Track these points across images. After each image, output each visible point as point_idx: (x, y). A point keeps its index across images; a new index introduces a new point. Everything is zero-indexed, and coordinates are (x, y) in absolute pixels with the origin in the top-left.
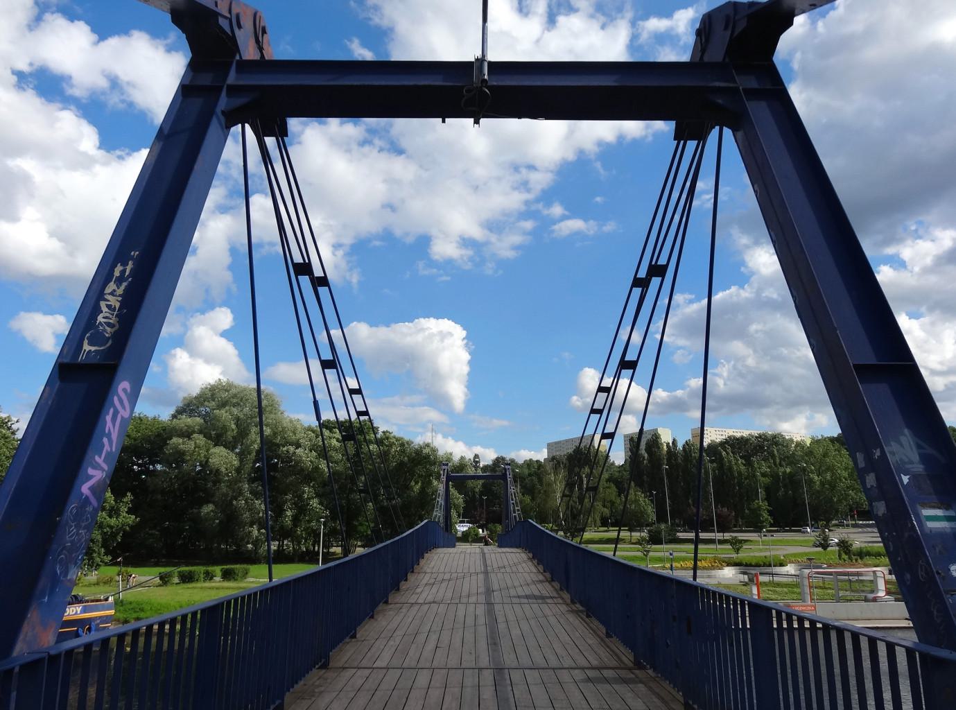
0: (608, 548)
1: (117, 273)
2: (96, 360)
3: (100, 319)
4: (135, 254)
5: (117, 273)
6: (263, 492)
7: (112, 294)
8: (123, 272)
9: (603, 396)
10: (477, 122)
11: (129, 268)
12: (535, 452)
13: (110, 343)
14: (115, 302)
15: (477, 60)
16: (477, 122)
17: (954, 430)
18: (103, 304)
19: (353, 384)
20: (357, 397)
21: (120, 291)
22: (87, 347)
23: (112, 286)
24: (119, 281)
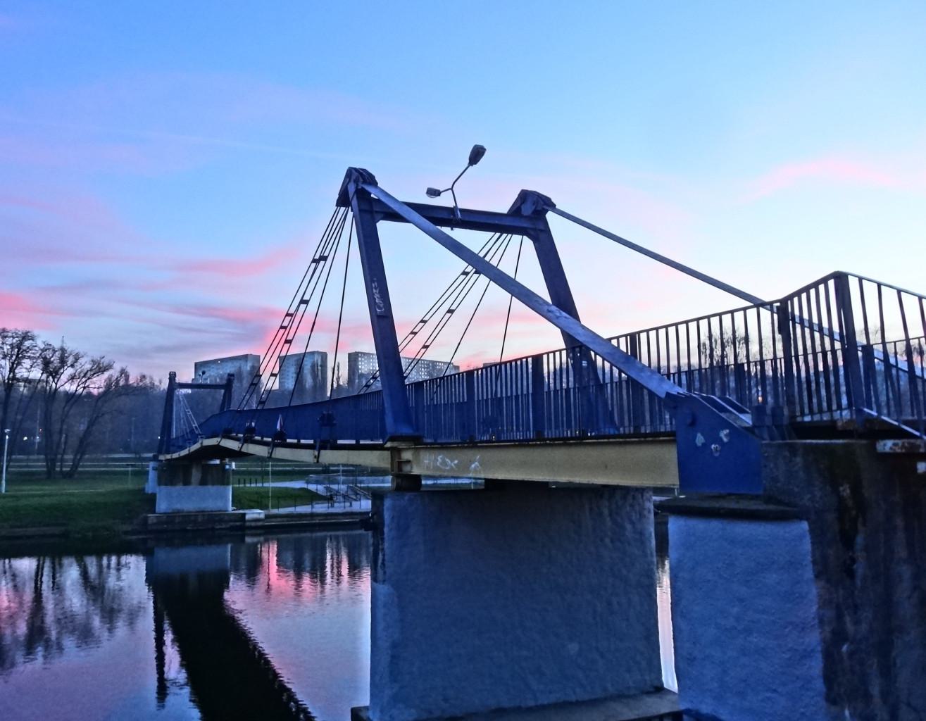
10: (452, 229)
21: (378, 292)
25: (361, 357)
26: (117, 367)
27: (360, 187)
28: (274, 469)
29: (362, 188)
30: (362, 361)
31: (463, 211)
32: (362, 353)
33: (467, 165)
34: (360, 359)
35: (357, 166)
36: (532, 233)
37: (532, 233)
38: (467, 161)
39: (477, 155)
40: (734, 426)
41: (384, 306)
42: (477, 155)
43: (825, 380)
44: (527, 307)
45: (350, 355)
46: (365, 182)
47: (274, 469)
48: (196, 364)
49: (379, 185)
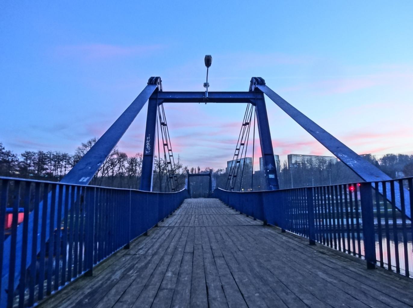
0: (80, 250)
1: (147, 139)
2: (148, 154)
3: (147, 147)
4: (149, 135)
5: (147, 139)
6: (241, 187)
7: (148, 142)
8: (148, 138)
9: (238, 151)
10: (206, 104)
11: (149, 137)
12: (409, 276)
13: (150, 151)
14: (148, 144)
15: (206, 91)
16: (206, 104)
17: (412, 156)
18: (147, 144)
19: (170, 149)
20: (170, 152)
21: (149, 142)
22: (147, 152)
23: (147, 141)
24: (148, 140)
25: (293, 156)
26: (184, 167)
27: (256, 87)
28: (313, 189)
29: (257, 87)
30: (293, 158)
31: (209, 93)
32: (293, 155)
33: (207, 68)
34: (293, 157)
35: (256, 76)
36: (252, 100)
37: (252, 100)
38: (206, 68)
39: (208, 61)
40: (63, 262)
41: (150, 150)
42: (208, 61)
43: (346, 192)
44: (312, 136)
45: (288, 156)
46: (258, 84)
47: (313, 189)
48: (228, 162)
49: (266, 84)
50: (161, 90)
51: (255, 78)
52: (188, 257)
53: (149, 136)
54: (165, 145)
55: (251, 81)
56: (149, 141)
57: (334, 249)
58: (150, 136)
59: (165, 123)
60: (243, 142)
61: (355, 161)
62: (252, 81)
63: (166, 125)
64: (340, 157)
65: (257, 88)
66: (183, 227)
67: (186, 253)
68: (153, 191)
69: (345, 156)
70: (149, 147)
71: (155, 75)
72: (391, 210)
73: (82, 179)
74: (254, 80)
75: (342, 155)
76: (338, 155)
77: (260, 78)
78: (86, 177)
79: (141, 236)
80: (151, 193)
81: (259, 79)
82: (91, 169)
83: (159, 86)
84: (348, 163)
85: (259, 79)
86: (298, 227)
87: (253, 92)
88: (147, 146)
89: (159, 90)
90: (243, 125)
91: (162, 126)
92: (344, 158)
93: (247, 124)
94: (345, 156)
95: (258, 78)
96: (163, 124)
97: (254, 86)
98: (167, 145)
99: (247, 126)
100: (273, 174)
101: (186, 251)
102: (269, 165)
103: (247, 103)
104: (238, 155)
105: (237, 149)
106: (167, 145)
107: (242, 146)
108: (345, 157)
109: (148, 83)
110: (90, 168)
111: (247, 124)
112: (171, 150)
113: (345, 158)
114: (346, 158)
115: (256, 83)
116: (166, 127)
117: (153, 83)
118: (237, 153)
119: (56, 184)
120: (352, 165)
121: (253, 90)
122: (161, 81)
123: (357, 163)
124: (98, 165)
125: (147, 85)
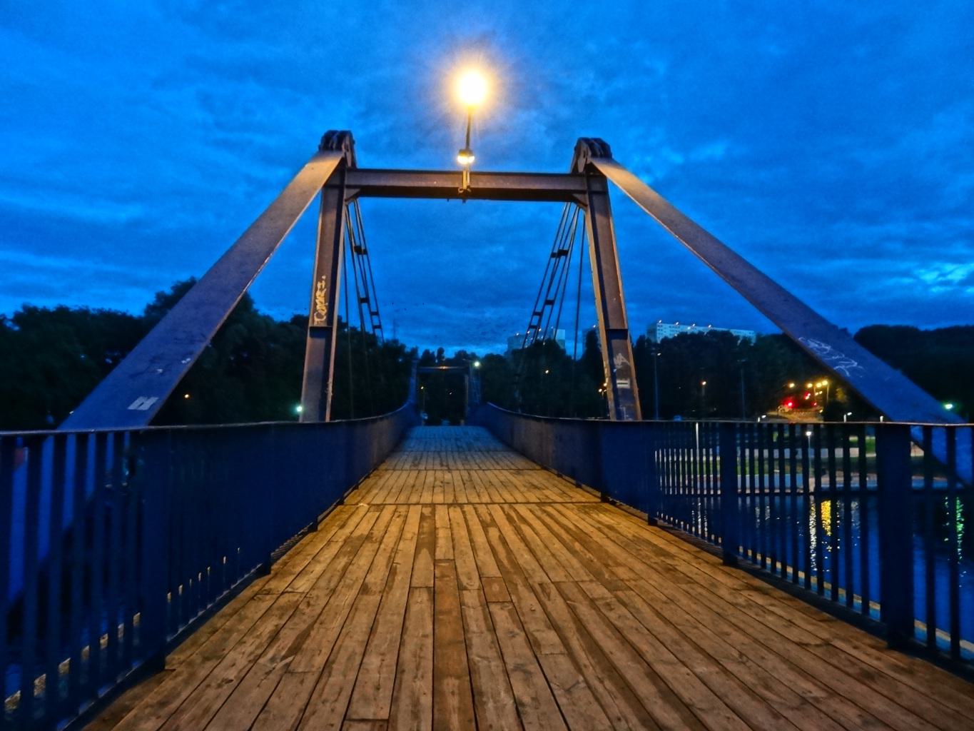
3: (318, 307)
5: (319, 287)
8: (321, 286)
19: (374, 309)
20: (375, 318)
27: (588, 162)
46: (594, 155)
49: (613, 157)
50: (354, 164)
51: (587, 140)
52: (422, 598)
53: (322, 280)
54: (362, 301)
55: (576, 149)
56: (324, 292)
57: (616, 420)
58: (326, 281)
59: (363, 248)
60: (551, 297)
61: (853, 362)
62: (578, 149)
63: (365, 252)
64: (815, 349)
65: (591, 164)
66: (405, 507)
67: (416, 588)
68: (331, 419)
69: (827, 348)
70: (324, 308)
71: (340, 127)
72: (875, 455)
73: (138, 402)
74: (585, 147)
75: (819, 345)
76: (809, 345)
77: (598, 140)
78: (149, 398)
79: (304, 534)
80: (328, 423)
81: (596, 144)
82: (162, 374)
83: (349, 155)
84: (837, 367)
85: (596, 144)
86: (671, 493)
87: (581, 175)
88: (317, 304)
89: (349, 164)
90: (553, 255)
91: (355, 254)
92: (825, 353)
93: (563, 253)
94: (827, 348)
95: (593, 141)
96: (359, 250)
97: (585, 160)
98: (366, 300)
99: (563, 258)
100: (626, 379)
101: (416, 582)
102: (618, 357)
103: (566, 203)
104: (536, 327)
105: (535, 313)
106: (366, 300)
107: (548, 308)
108: (825, 350)
109: (320, 148)
110: (160, 370)
111: (563, 253)
112: (377, 313)
113: (827, 354)
114: (830, 354)
115: (590, 153)
116: (365, 256)
117: (334, 147)
118: (535, 322)
119: (44, 437)
120: (848, 374)
121: (581, 169)
122: (352, 142)
123: (860, 367)
124: (183, 362)
125: (317, 150)
